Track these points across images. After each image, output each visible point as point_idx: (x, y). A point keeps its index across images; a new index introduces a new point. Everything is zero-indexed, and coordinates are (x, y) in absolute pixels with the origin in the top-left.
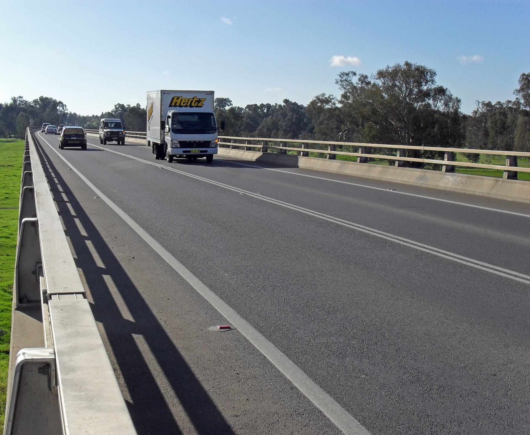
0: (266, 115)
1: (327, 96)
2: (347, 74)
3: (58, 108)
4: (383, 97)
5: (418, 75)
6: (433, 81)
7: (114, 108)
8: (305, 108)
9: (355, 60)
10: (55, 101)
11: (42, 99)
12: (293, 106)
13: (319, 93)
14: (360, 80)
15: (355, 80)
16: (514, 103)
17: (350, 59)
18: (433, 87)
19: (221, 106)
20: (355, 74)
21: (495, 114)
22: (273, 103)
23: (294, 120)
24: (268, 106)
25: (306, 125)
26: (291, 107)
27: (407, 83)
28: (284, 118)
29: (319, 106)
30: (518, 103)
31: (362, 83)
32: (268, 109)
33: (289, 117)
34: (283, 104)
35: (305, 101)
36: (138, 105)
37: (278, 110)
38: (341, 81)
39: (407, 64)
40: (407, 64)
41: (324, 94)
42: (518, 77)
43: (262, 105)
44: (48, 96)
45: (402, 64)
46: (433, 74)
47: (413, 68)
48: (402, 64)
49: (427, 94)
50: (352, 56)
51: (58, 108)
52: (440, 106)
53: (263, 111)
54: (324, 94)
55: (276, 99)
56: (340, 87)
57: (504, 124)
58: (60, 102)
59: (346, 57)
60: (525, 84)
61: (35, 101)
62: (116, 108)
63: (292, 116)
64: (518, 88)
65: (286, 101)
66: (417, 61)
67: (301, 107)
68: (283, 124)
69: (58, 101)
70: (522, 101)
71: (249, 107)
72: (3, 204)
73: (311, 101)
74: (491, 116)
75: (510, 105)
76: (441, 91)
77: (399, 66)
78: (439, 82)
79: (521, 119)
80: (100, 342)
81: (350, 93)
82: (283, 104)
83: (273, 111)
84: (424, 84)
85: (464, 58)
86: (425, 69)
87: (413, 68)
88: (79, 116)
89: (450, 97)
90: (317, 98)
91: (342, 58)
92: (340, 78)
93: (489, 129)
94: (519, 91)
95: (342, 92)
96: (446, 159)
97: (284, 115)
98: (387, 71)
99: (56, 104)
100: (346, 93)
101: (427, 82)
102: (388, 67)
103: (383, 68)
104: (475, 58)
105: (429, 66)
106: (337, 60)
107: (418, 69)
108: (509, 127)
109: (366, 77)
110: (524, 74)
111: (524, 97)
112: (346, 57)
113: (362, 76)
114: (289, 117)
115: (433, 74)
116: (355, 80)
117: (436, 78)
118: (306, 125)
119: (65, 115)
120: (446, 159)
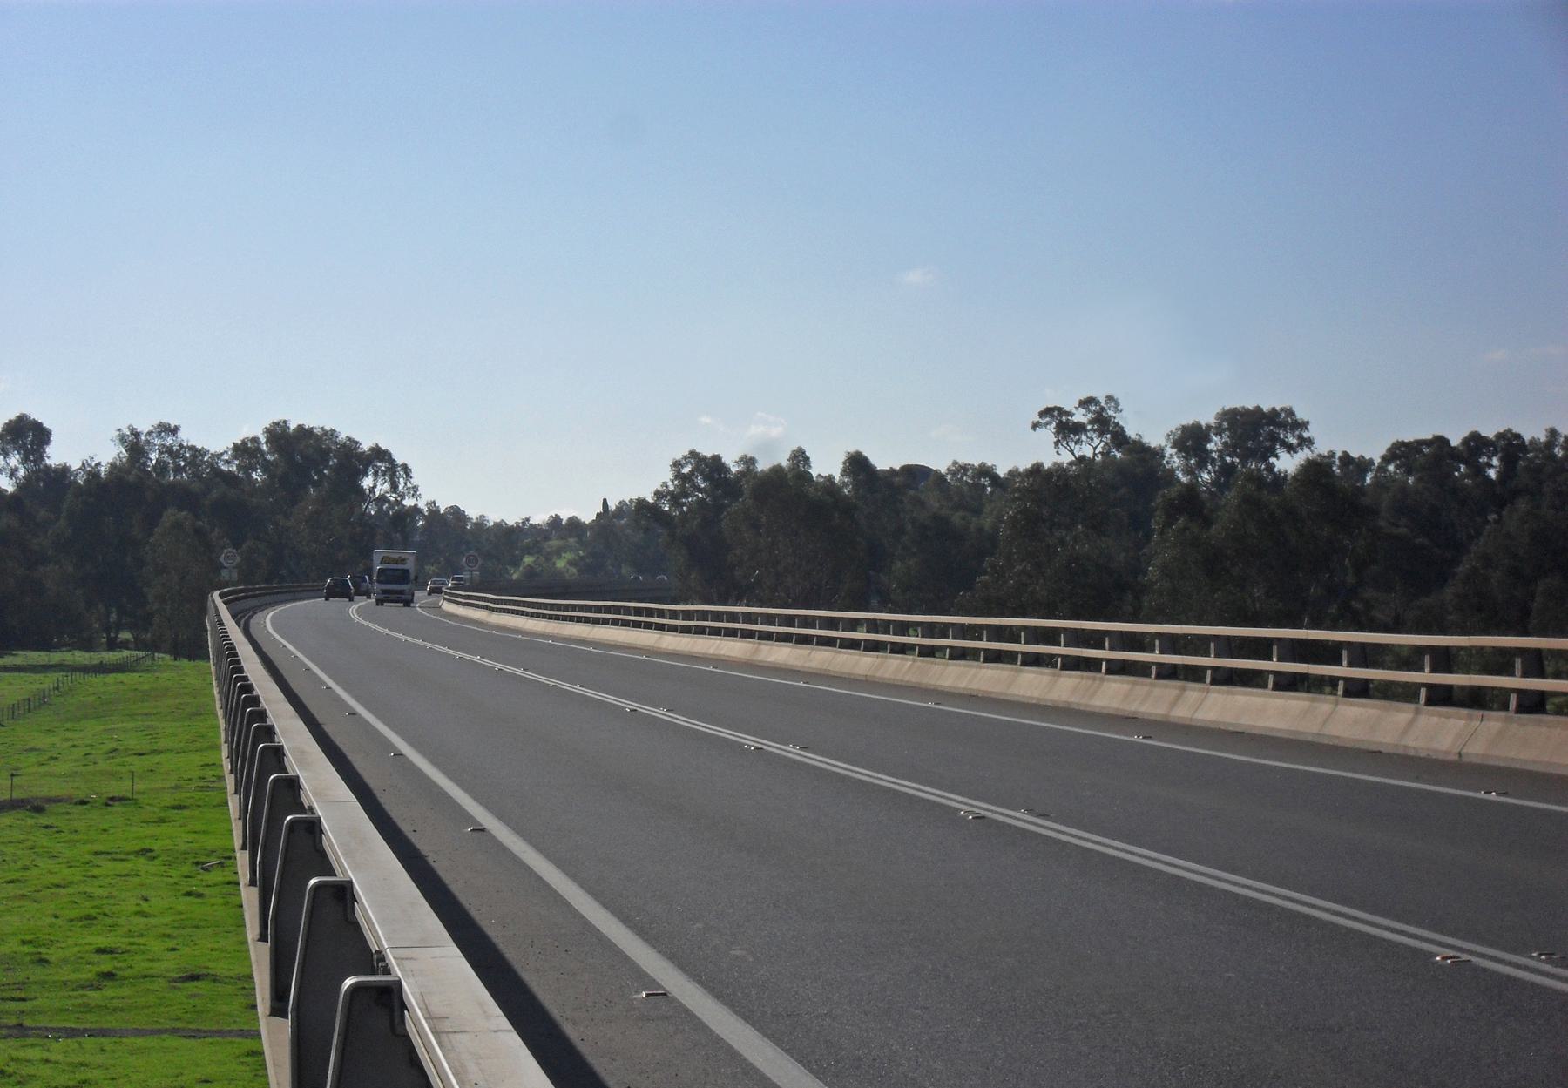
3: (367, 482)
10: (350, 448)
11: (279, 435)
24: (1510, 445)
51: (367, 482)
58: (379, 454)
61: (1192, 440)
62: (678, 476)
69: (366, 446)
72: (88, 1008)
99: (352, 461)
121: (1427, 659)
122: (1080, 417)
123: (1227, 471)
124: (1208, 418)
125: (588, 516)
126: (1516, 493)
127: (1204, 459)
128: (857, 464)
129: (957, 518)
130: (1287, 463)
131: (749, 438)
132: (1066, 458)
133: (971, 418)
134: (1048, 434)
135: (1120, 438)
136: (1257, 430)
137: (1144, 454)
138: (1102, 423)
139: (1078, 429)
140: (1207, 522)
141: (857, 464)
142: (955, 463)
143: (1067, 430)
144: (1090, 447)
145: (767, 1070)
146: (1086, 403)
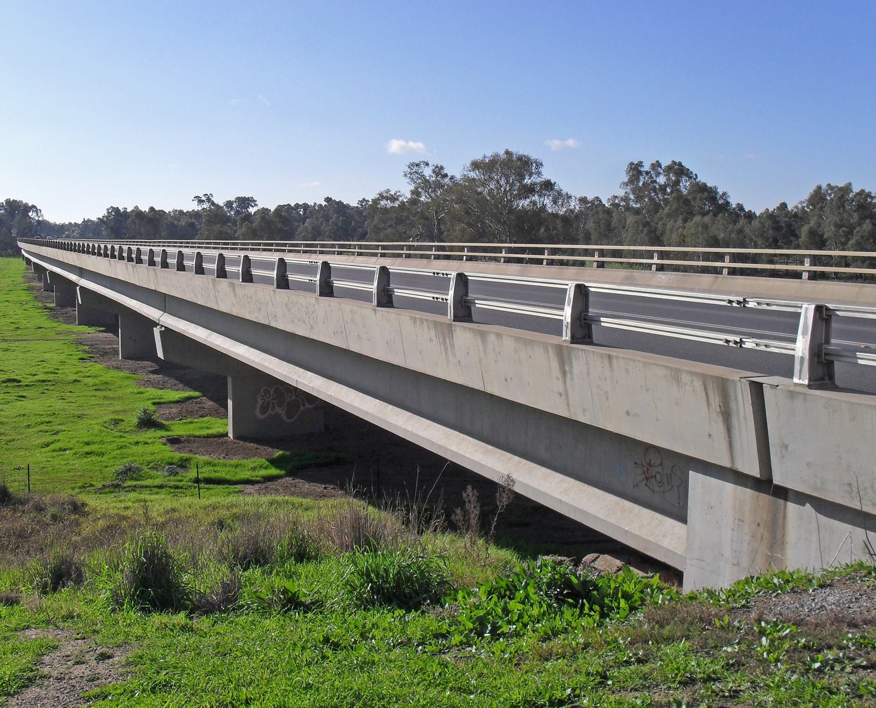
0: (303, 219)
1: (392, 193)
3: (30, 214)
5: (520, 165)
6: (539, 174)
7: (105, 213)
8: (353, 208)
9: (420, 145)
10: (26, 205)
11: (8, 202)
13: (382, 189)
14: (434, 172)
15: (428, 172)
16: (622, 199)
17: (411, 144)
18: (539, 180)
19: (243, 208)
20: (427, 164)
21: (597, 213)
22: (311, 203)
23: (340, 224)
24: (305, 206)
25: (355, 229)
26: (335, 207)
27: (507, 178)
28: (328, 221)
30: (626, 199)
31: (437, 176)
32: (305, 211)
33: (333, 220)
34: (324, 203)
36: (136, 207)
37: (318, 211)
38: (411, 174)
39: (507, 152)
40: (507, 152)
41: (388, 190)
42: (625, 166)
45: (501, 152)
46: (539, 165)
47: (514, 158)
48: (501, 152)
49: (529, 190)
50: (415, 141)
51: (30, 214)
52: (389, 204)
54: (388, 190)
55: (316, 198)
56: (408, 180)
57: (608, 224)
58: (33, 206)
59: (407, 141)
60: (634, 175)
61: (229, 204)
62: (108, 212)
64: (626, 180)
65: (328, 200)
66: (519, 150)
67: (347, 207)
68: (325, 228)
69: (30, 205)
70: (632, 197)
72: (18, 335)
74: (593, 215)
75: (617, 201)
76: (548, 185)
77: (497, 155)
78: (547, 174)
79: (631, 219)
80: (364, 408)
81: (422, 188)
82: (324, 203)
84: (527, 177)
85: (557, 142)
86: (529, 159)
87: (514, 158)
89: (559, 193)
90: (380, 195)
91: (402, 143)
92: (409, 170)
93: (592, 231)
94: (626, 184)
95: (412, 187)
96: (596, 256)
97: (327, 218)
98: (482, 162)
99: (27, 208)
100: (416, 188)
101: (531, 175)
102: (485, 157)
103: (478, 157)
104: (571, 142)
105: (533, 154)
106: (395, 145)
107: (520, 158)
108: (615, 228)
109: (442, 168)
110: (632, 164)
111: (634, 191)
112: (407, 141)
113: (437, 167)
114: (333, 220)
115: (539, 165)
116: (428, 172)
117: (542, 170)
118: (355, 229)
120: (596, 256)
121: (655, 254)
122: (204, 198)
123: (237, 212)
124: (233, 199)
125: (80, 222)
126: (307, 218)
127: (232, 208)
128: (152, 209)
129: (175, 222)
130: (252, 210)
131: (127, 204)
132: (200, 208)
133: (176, 198)
134: (196, 202)
135: (213, 204)
136: (245, 202)
137: (218, 206)
138: (209, 200)
139: (203, 201)
140: (251, 223)
141: (152, 209)
142: (136, 207)
143: (200, 201)
144: (206, 206)
145: (215, 335)
146: (205, 195)
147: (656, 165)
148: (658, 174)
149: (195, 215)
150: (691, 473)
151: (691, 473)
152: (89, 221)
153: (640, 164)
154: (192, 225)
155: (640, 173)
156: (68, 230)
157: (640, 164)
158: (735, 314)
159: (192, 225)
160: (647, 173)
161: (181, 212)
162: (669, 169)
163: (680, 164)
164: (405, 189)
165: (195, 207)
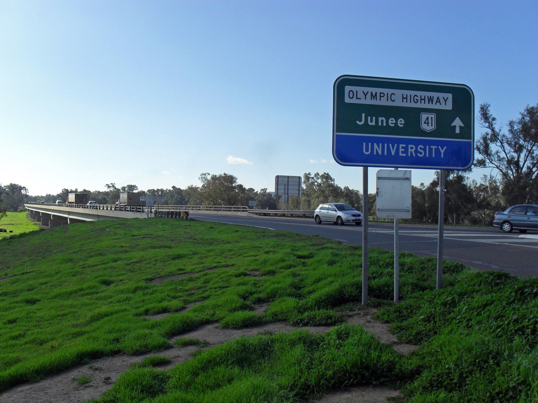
2: (205, 174)
4: (510, 177)
12: (220, 180)
22: (165, 189)
24: (162, 190)
26: (177, 191)
29: (192, 190)
32: (162, 193)
34: (171, 189)
35: (183, 186)
37: (168, 193)
39: (225, 174)
40: (225, 174)
43: (158, 190)
44: (16, 183)
45: (222, 174)
48: (222, 174)
51: (22, 191)
53: (158, 193)
55: (167, 186)
58: (24, 187)
63: (177, 197)
65: (174, 187)
66: (229, 173)
71: (149, 191)
73: (431, 181)
82: (171, 189)
83: (165, 193)
88: (31, 197)
97: (172, 196)
99: (21, 188)
105: (235, 175)
110: (306, 174)
119: (27, 196)
122: (111, 185)
124: (126, 186)
125: (44, 195)
132: (108, 190)
135: (115, 188)
138: (113, 186)
143: (109, 187)
144: (112, 189)
147: (317, 175)
148: (318, 178)
149: (106, 194)
150: (458, 118)
151: (458, 118)
152: (50, 195)
153: (309, 174)
154: (105, 199)
155: (309, 178)
156: (39, 199)
157: (309, 174)
158: (456, 168)
159: (105, 199)
160: (313, 178)
161: (99, 192)
162: (322, 176)
163: (328, 174)
164: (199, 184)
165: (106, 189)
